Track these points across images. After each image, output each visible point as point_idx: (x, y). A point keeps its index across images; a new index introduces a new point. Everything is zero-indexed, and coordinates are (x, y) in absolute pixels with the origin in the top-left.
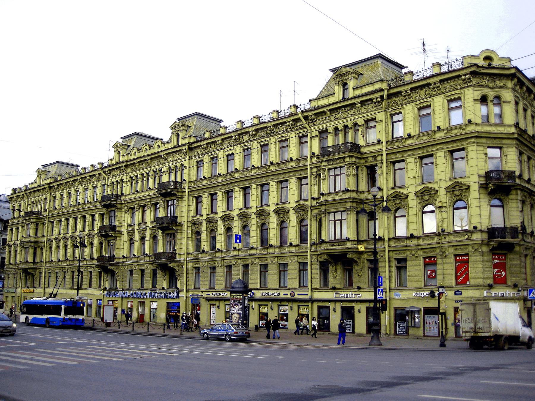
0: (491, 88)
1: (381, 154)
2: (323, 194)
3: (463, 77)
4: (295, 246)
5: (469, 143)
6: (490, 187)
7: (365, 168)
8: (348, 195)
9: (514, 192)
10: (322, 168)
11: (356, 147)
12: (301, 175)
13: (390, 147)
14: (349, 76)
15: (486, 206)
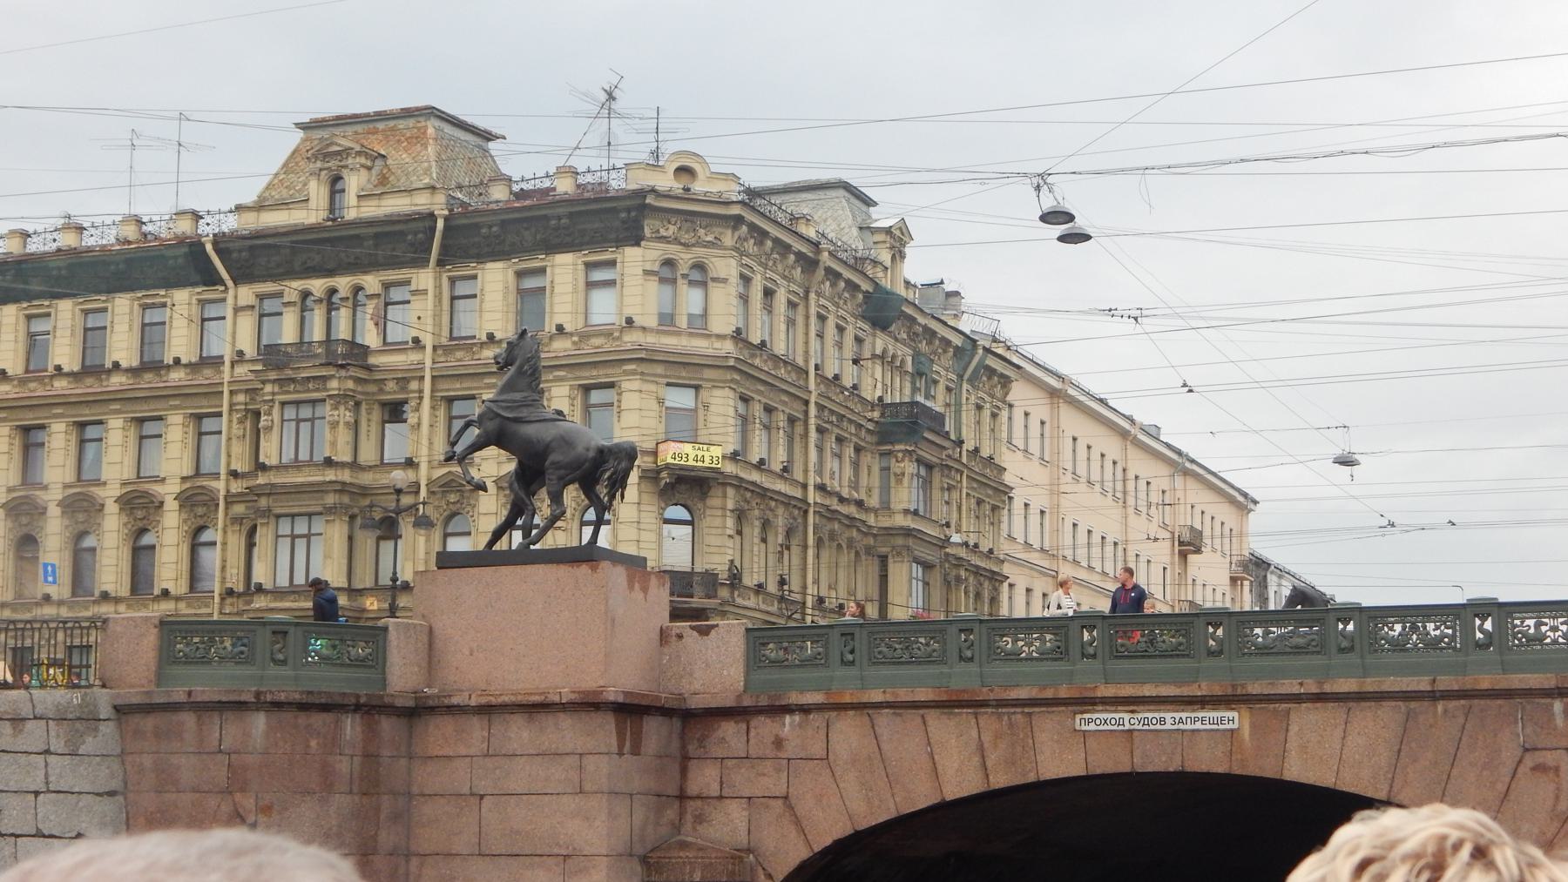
0: (685, 245)
1: (418, 375)
2: (263, 468)
3: (623, 215)
4: (178, 599)
5: (626, 373)
6: (664, 478)
7: (376, 407)
8: (330, 475)
9: (716, 491)
10: (266, 398)
11: (357, 353)
12: (201, 407)
13: (442, 359)
14: (350, 161)
15: (654, 521)
